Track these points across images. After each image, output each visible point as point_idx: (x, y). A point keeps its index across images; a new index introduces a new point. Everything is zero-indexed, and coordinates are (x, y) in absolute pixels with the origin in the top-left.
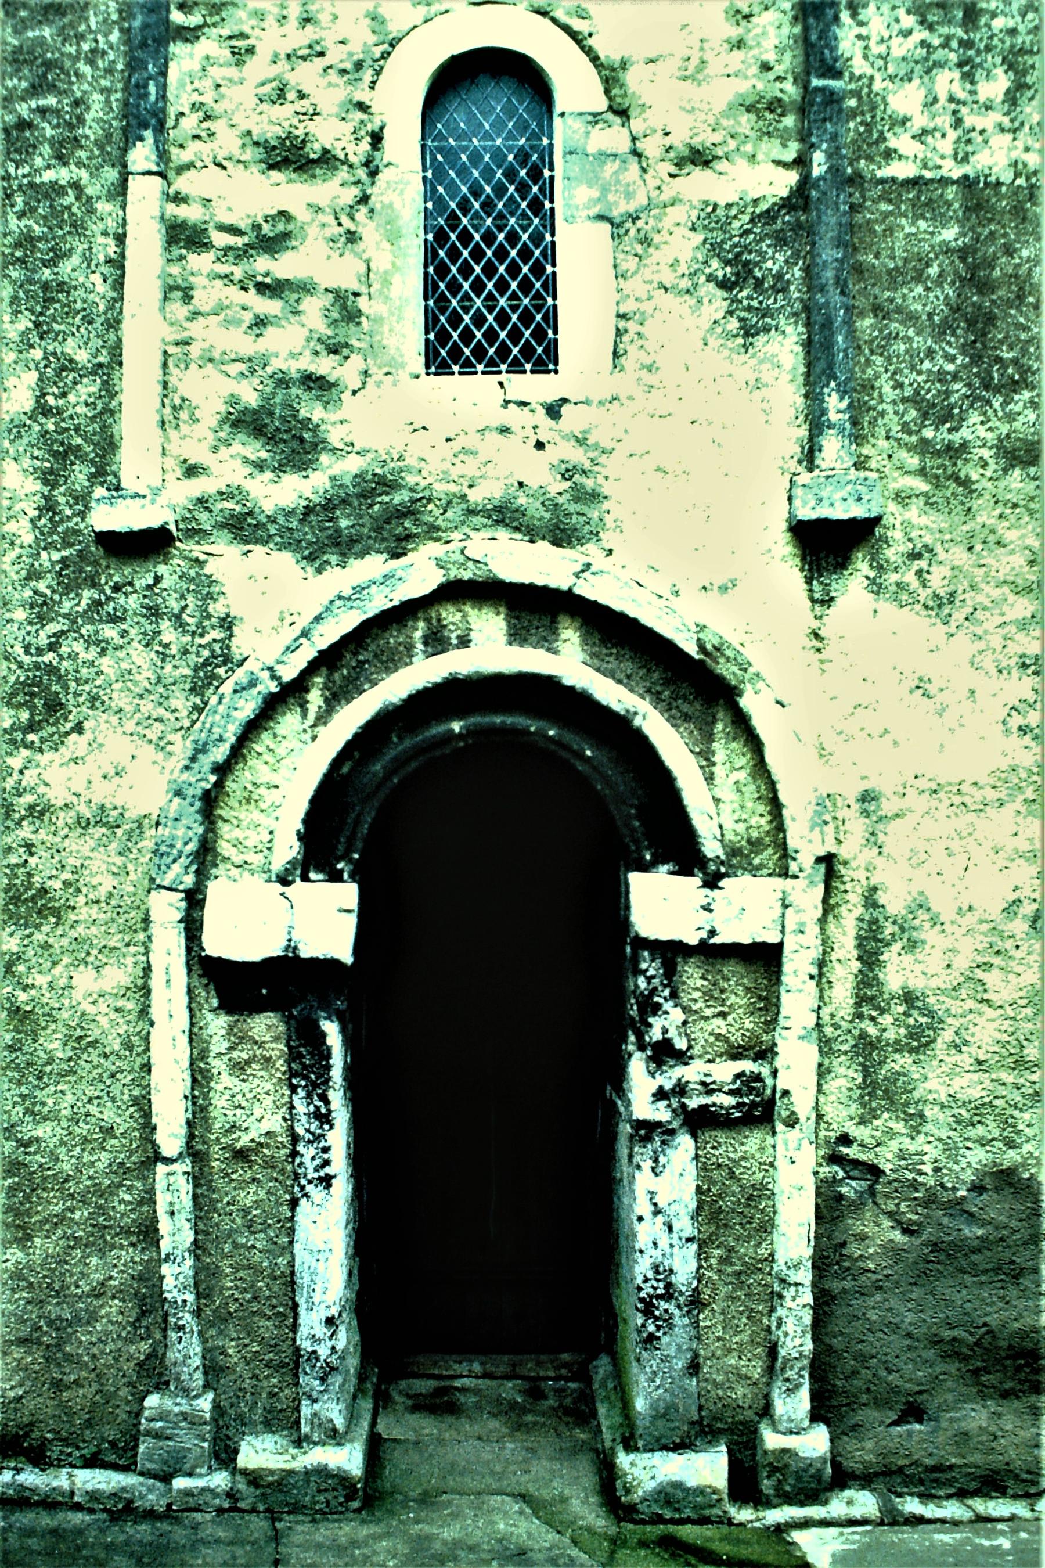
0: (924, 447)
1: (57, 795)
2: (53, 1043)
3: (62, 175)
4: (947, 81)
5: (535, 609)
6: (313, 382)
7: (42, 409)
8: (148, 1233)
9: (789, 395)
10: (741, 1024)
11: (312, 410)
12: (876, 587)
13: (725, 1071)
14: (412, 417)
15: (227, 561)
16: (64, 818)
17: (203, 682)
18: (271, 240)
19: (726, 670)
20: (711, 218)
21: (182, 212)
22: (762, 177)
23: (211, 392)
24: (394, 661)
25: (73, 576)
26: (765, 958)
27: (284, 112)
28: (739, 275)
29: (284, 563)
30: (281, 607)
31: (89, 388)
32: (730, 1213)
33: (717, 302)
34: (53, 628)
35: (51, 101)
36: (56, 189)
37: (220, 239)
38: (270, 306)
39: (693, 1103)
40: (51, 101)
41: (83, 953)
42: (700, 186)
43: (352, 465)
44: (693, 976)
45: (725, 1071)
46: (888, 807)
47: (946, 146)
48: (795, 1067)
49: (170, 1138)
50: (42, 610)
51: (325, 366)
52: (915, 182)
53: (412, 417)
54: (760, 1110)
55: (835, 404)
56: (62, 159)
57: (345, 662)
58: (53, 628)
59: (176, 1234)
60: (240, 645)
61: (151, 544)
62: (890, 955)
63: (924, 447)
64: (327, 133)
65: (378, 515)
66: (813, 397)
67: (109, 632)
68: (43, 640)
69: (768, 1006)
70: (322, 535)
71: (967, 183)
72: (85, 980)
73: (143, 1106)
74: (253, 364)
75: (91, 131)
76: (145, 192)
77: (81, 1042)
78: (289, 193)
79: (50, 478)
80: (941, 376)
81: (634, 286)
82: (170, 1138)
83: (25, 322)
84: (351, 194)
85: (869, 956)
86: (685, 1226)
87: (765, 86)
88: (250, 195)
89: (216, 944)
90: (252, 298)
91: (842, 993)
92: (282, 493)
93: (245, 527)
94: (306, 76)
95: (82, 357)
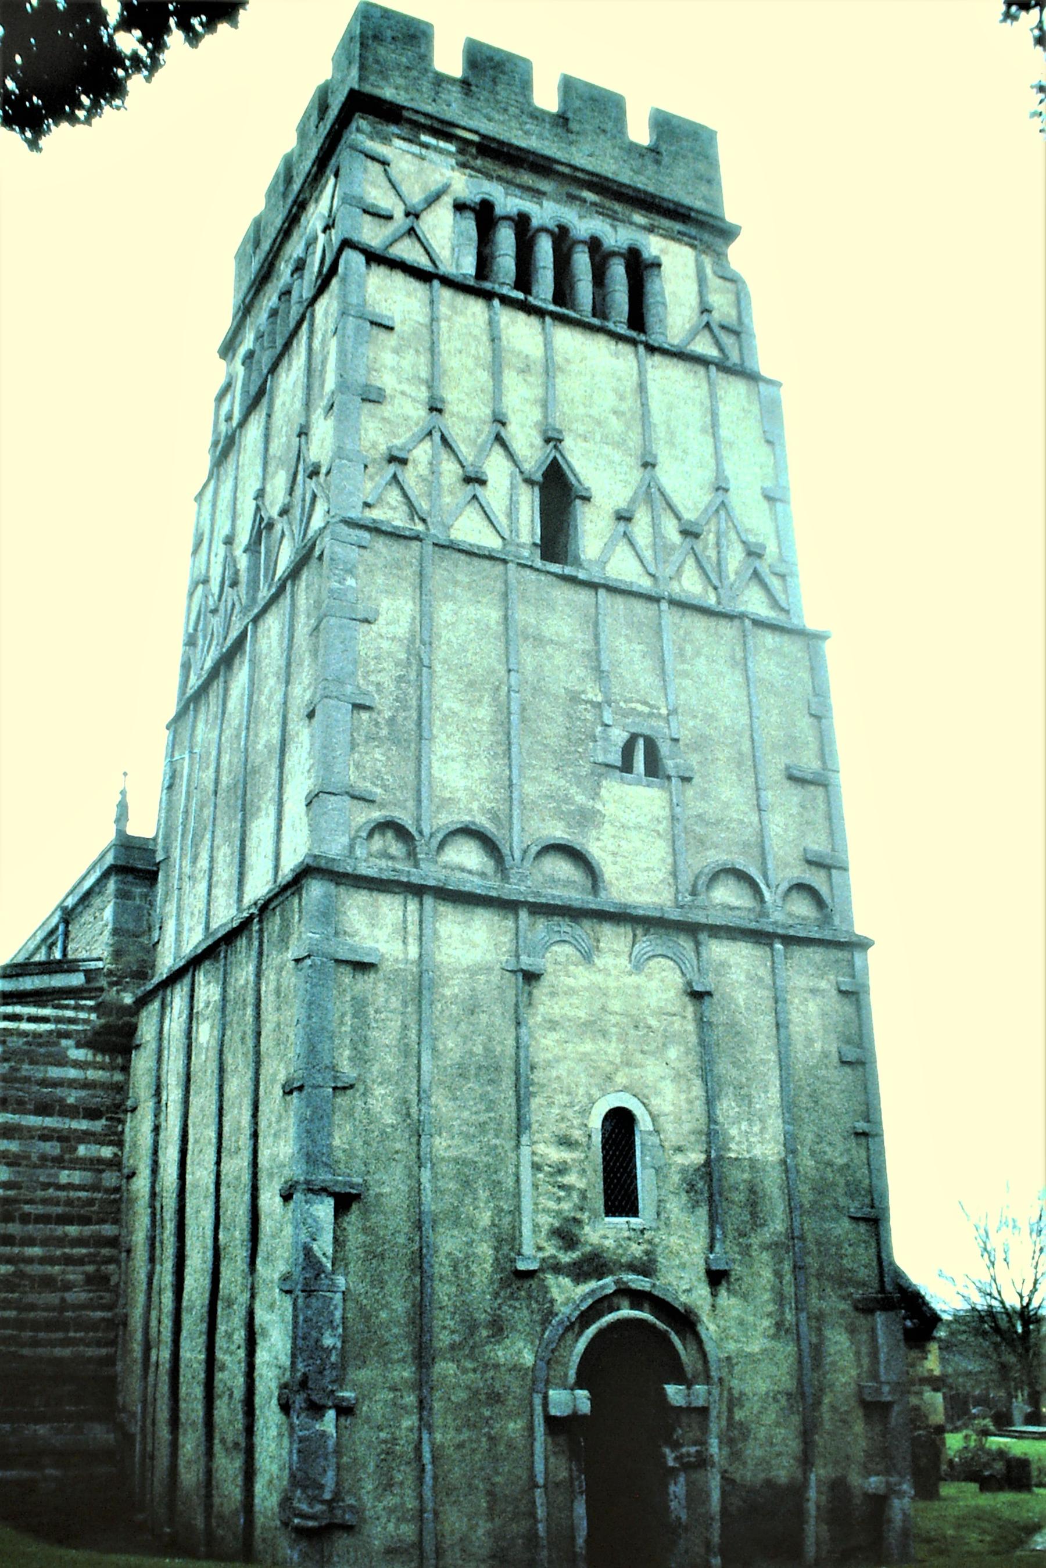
0: (739, 1244)
1: (502, 1361)
2: (502, 1448)
3: (498, 1142)
4: (744, 1126)
5: (638, 1298)
6: (575, 1219)
7: (494, 1225)
8: (532, 1514)
9: (704, 1229)
10: (695, 1434)
11: (575, 1230)
12: (728, 1290)
13: (693, 1450)
14: (605, 1232)
15: (550, 1279)
16: (503, 1369)
17: (545, 1321)
18: (562, 1169)
19: (693, 1317)
20: (683, 1170)
21: (536, 1159)
22: (696, 1157)
23: (546, 1221)
24: (601, 1315)
25: (504, 1284)
26: (704, 1411)
27: (563, 1125)
28: (691, 1188)
29: (566, 1281)
30: (567, 1294)
31: (509, 1218)
32: (696, 1496)
33: (684, 1197)
34: (499, 1301)
35: (492, 1115)
36: (496, 1147)
37: (546, 1168)
38: (562, 1194)
39: (685, 1460)
40: (492, 1115)
41: (510, 1416)
42: (679, 1159)
43: (588, 1249)
44: (685, 1420)
45: (693, 1450)
46: (734, 1361)
47: (744, 1147)
48: (714, 1447)
49: (540, 1480)
50: (496, 1295)
51: (579, 1216)
52: (736, 1159)
53: (605, 1232)
54: (702, 1462)
55: (718, 1232)
56: (497, 1136)
57: (586, 1318)
58: (499, 1301)
59: (541, 1513)
60: (556, 1309)
61: (530, 1274)
62: (736, 1410)
63: (739, 1244)
64: (577, 1134)
65: (593, 1265)
66: (712, 1228)
67: (517, 1304)
68: (496, 1305)
69: (705, 1430)
70: (581, 1271)
71: (750, 1159)
72: (511, 1425)
73: (531, 1468)
74: (559, 1213)
75: (505, 1127)
76: (525, 1151)
77: (510, 1446)
78: (566, 1155)
79: (497, 1249)
80: (743, 1222)
81: (663, 1192)
82: (540, 1480)
83: (487, 1193)
84: (583, 1155)
85: (730, 1411)
86: (683, 1502)
87: (700, 1127)
88: (555, 1154)
89: (553, 1412)
90: (556, 1190)
91: (724, 1423)
92: (566, 1258)
93: (557, 1269)
94: (569, 1113)
95: (505, 1207)
